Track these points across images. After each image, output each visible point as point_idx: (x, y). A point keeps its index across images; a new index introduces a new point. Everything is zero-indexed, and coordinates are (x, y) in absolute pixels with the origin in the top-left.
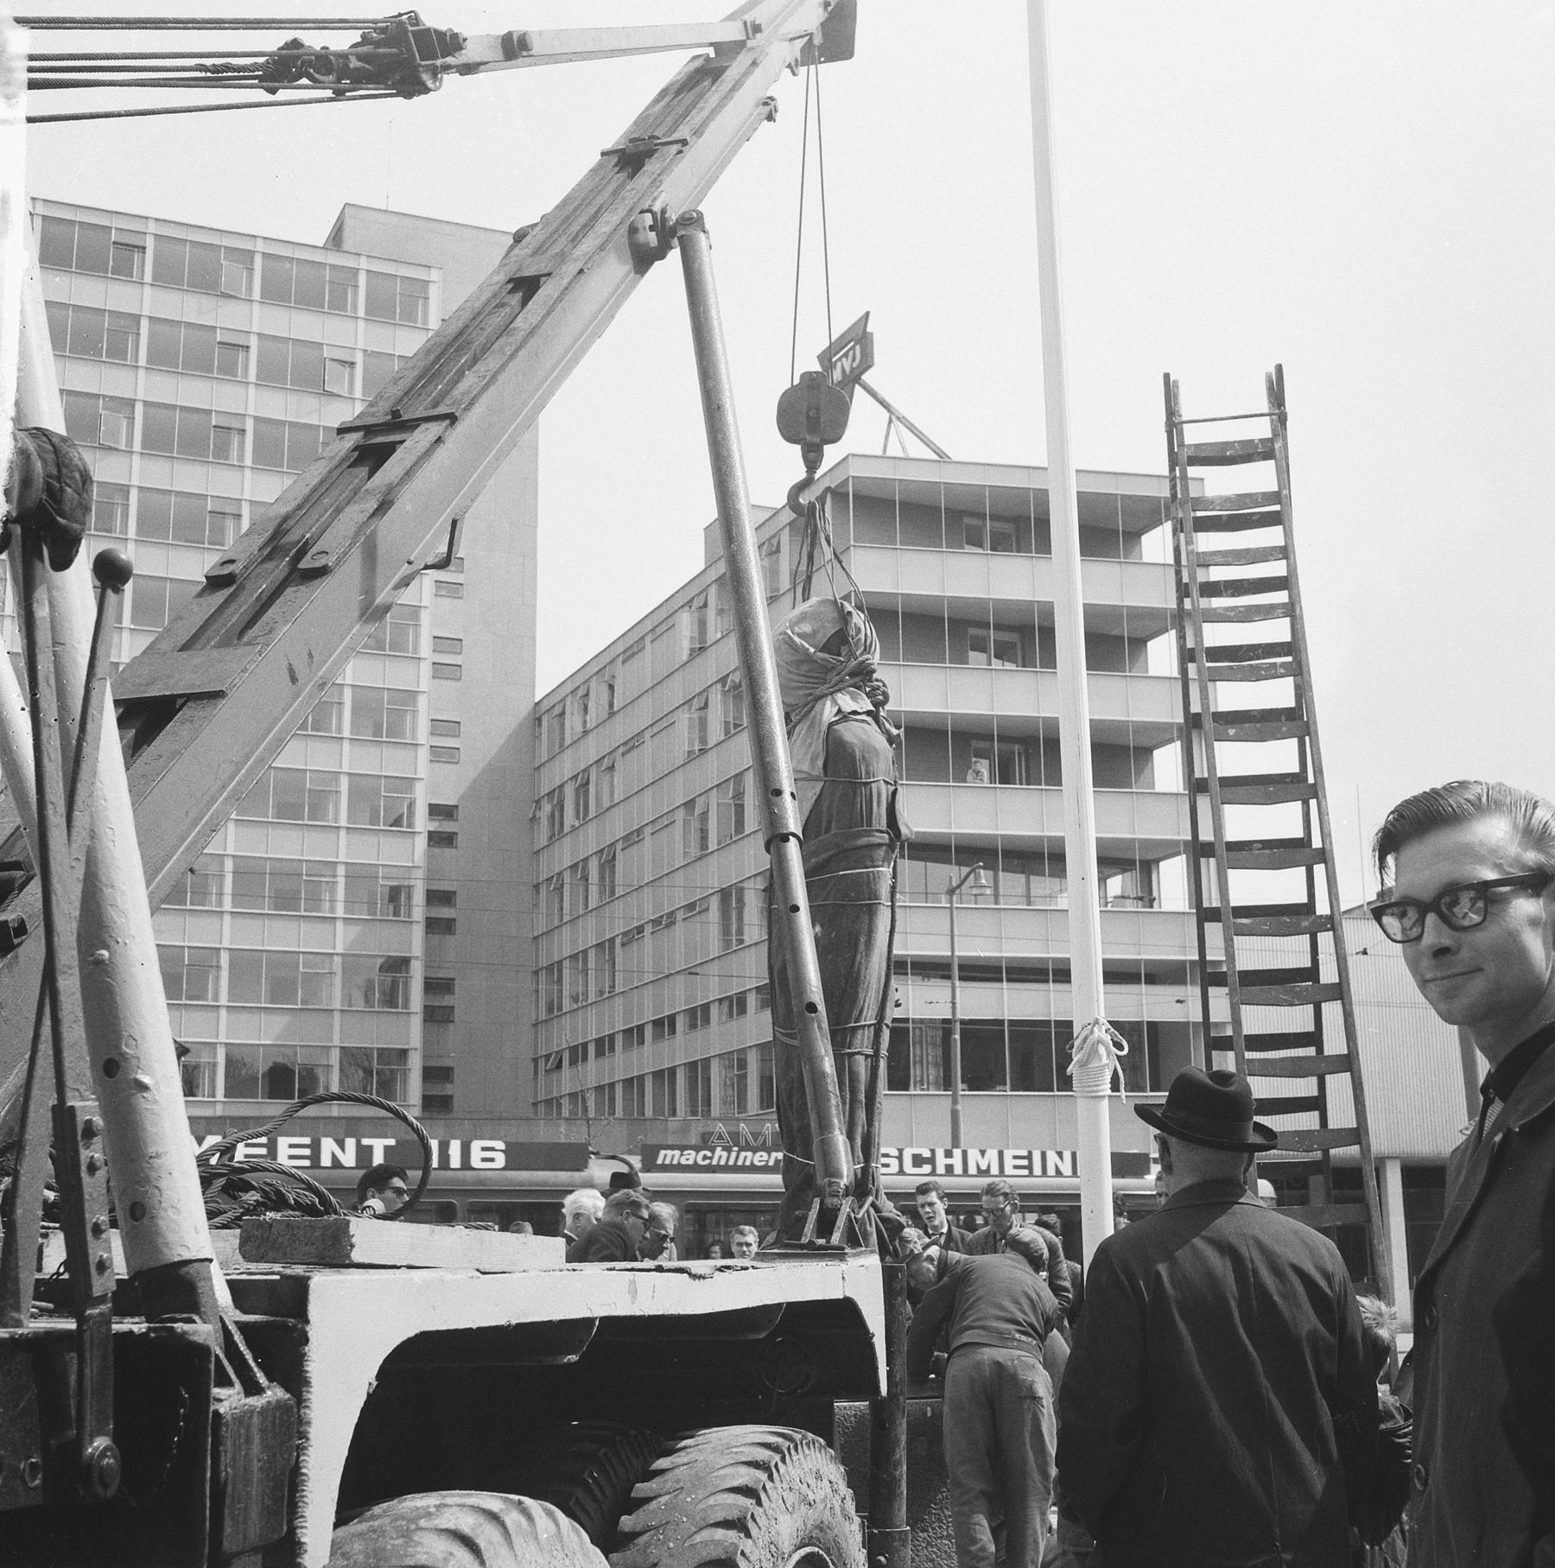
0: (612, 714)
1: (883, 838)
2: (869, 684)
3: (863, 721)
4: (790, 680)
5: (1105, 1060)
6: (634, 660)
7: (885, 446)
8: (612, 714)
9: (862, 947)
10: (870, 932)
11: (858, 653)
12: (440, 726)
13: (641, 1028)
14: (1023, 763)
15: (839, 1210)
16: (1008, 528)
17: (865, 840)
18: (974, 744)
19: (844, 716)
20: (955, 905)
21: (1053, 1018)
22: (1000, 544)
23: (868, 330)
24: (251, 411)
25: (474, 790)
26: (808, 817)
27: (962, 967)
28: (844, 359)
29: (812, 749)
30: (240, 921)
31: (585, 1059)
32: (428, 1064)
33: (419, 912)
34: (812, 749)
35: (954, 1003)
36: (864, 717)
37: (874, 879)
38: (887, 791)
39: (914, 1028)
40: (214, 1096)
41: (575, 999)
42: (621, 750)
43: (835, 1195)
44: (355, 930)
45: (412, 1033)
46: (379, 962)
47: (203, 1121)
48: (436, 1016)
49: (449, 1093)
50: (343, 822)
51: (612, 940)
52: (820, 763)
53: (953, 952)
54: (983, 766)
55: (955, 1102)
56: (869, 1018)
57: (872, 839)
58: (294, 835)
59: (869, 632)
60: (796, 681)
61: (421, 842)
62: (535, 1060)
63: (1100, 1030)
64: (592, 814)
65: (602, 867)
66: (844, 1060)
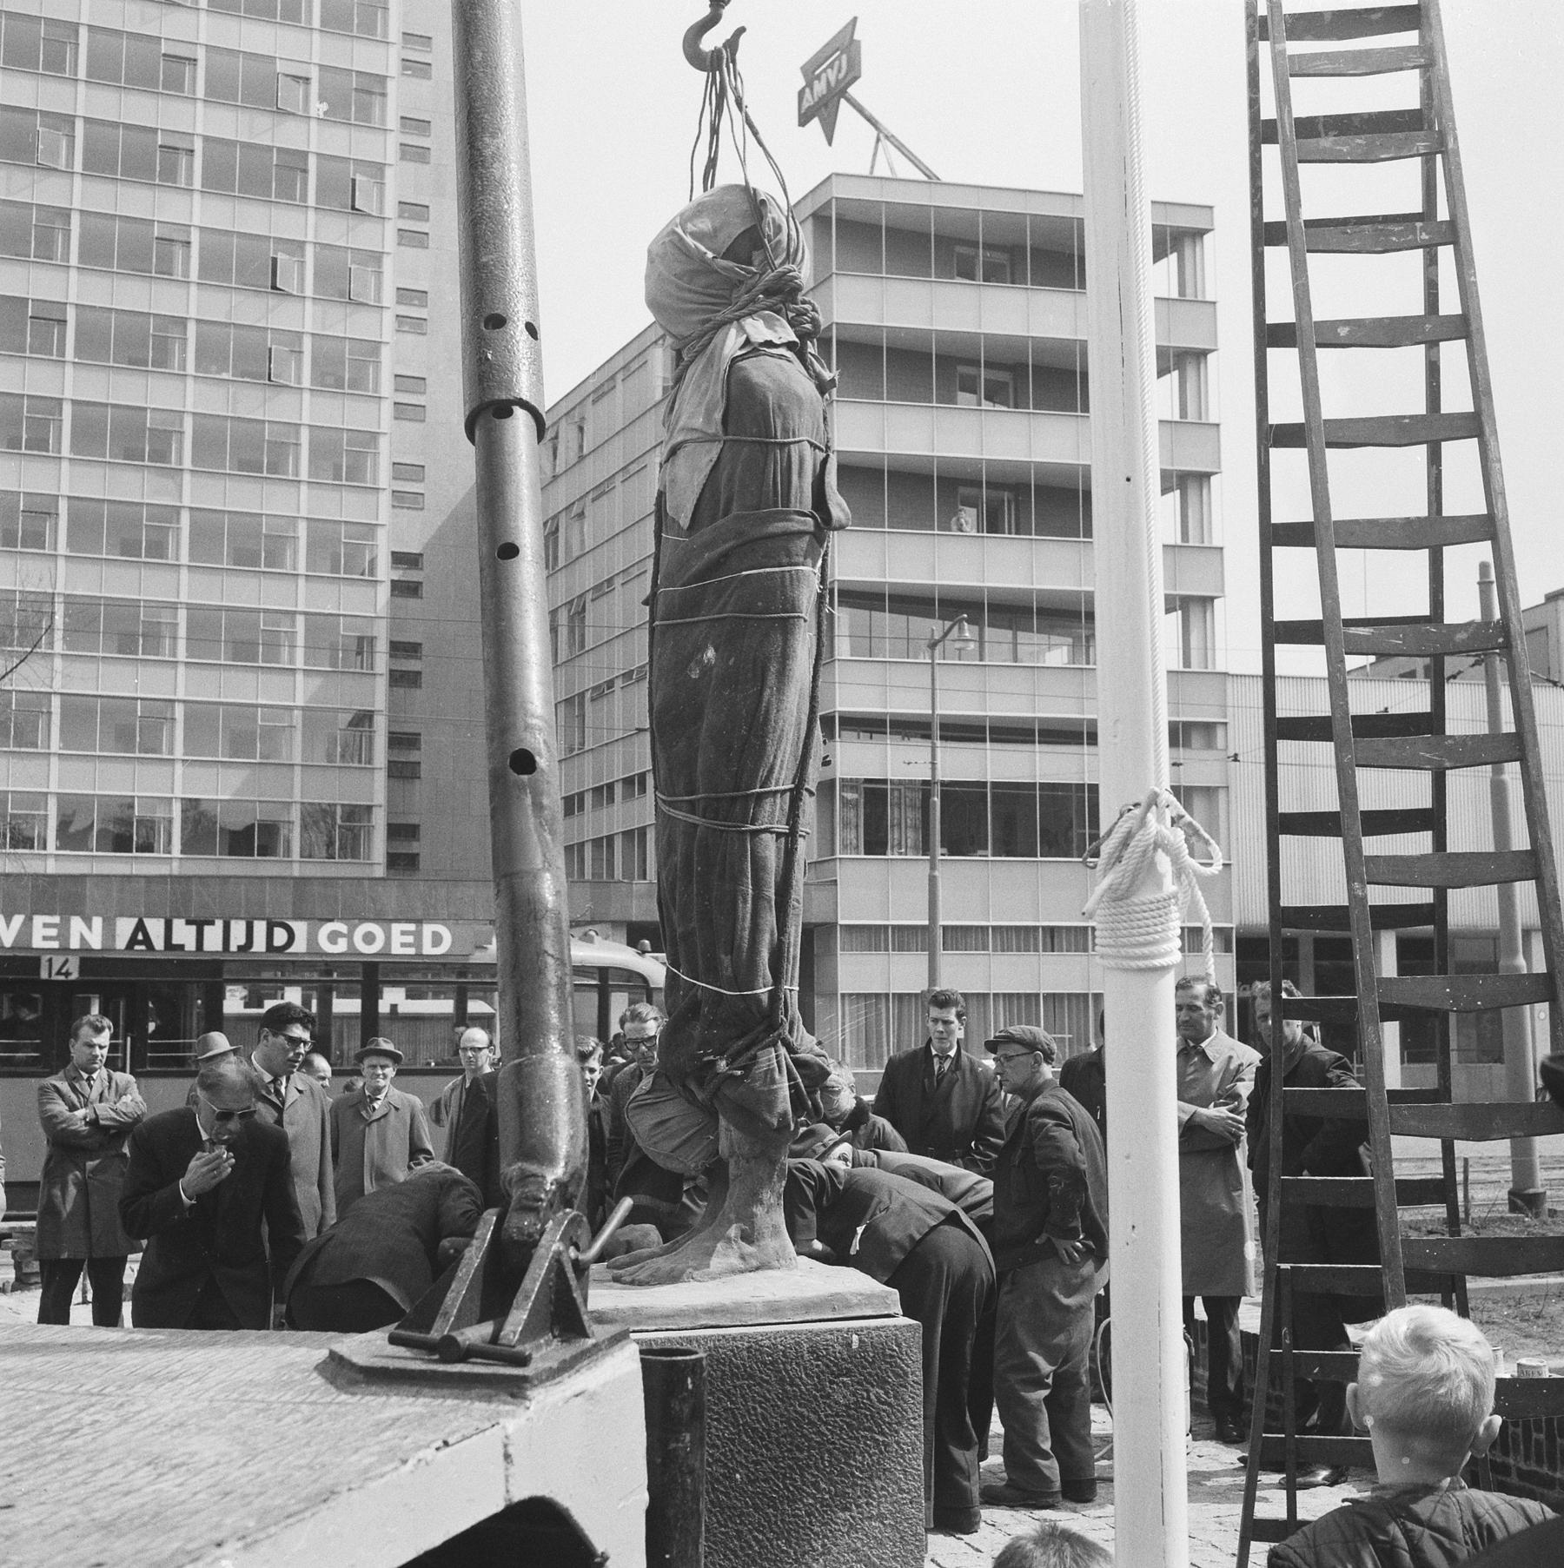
0: (582, 458)
1: (804, 523)
2: (792, 306)
3: (781, 357)
4: (686, 301)
5: (1169, 886)
6: (605, 399)
7: (872, 167)
8: (582, 458)
9: (772, 679)
10: (785, 658)
11: (777, 262)
12: (401, 470)
13: (610, 786)
14: (1013, 512)
15: (535, 1244)
16: (1000, 257)
17: (779, 526)
18: (962, 490)
19: (753, 349)
20: (937, 661)
21: (1038, 780)
22: (994, 274)
23: (856, 37)
24: (199, 130)
25: (440, 536)
26: (701, 494)
27: (943, 727)
28: (829, 70)
29: (708, 398)
30: (195, 672)
33: (382, 663)
34: (708, 398)
35: (933, 764)
36: (782, 351)
37: (791, 581)
38: (815, 460)
39: (892, 790)
40: (170, 853)
42: (591, 496)
43: (530, 1206)
44: (317, 682)
45: (376, 790)
46: (349, 717)
48: (401, 772)
49: (415, 851)
50: (302, 570)
51: (582, 695)
52: (718, 416)
53: (933, 709)
54: (968, 516)
55: (933, 868)
56: (783, 779)
57: (790, 524)
58: (252, 582)
59: (793, 233)
60: (691, 302)
61: (384, 592)
63: (1160, 819)
64: (561, 563)
65: (571, 619)
66: (744, 841)
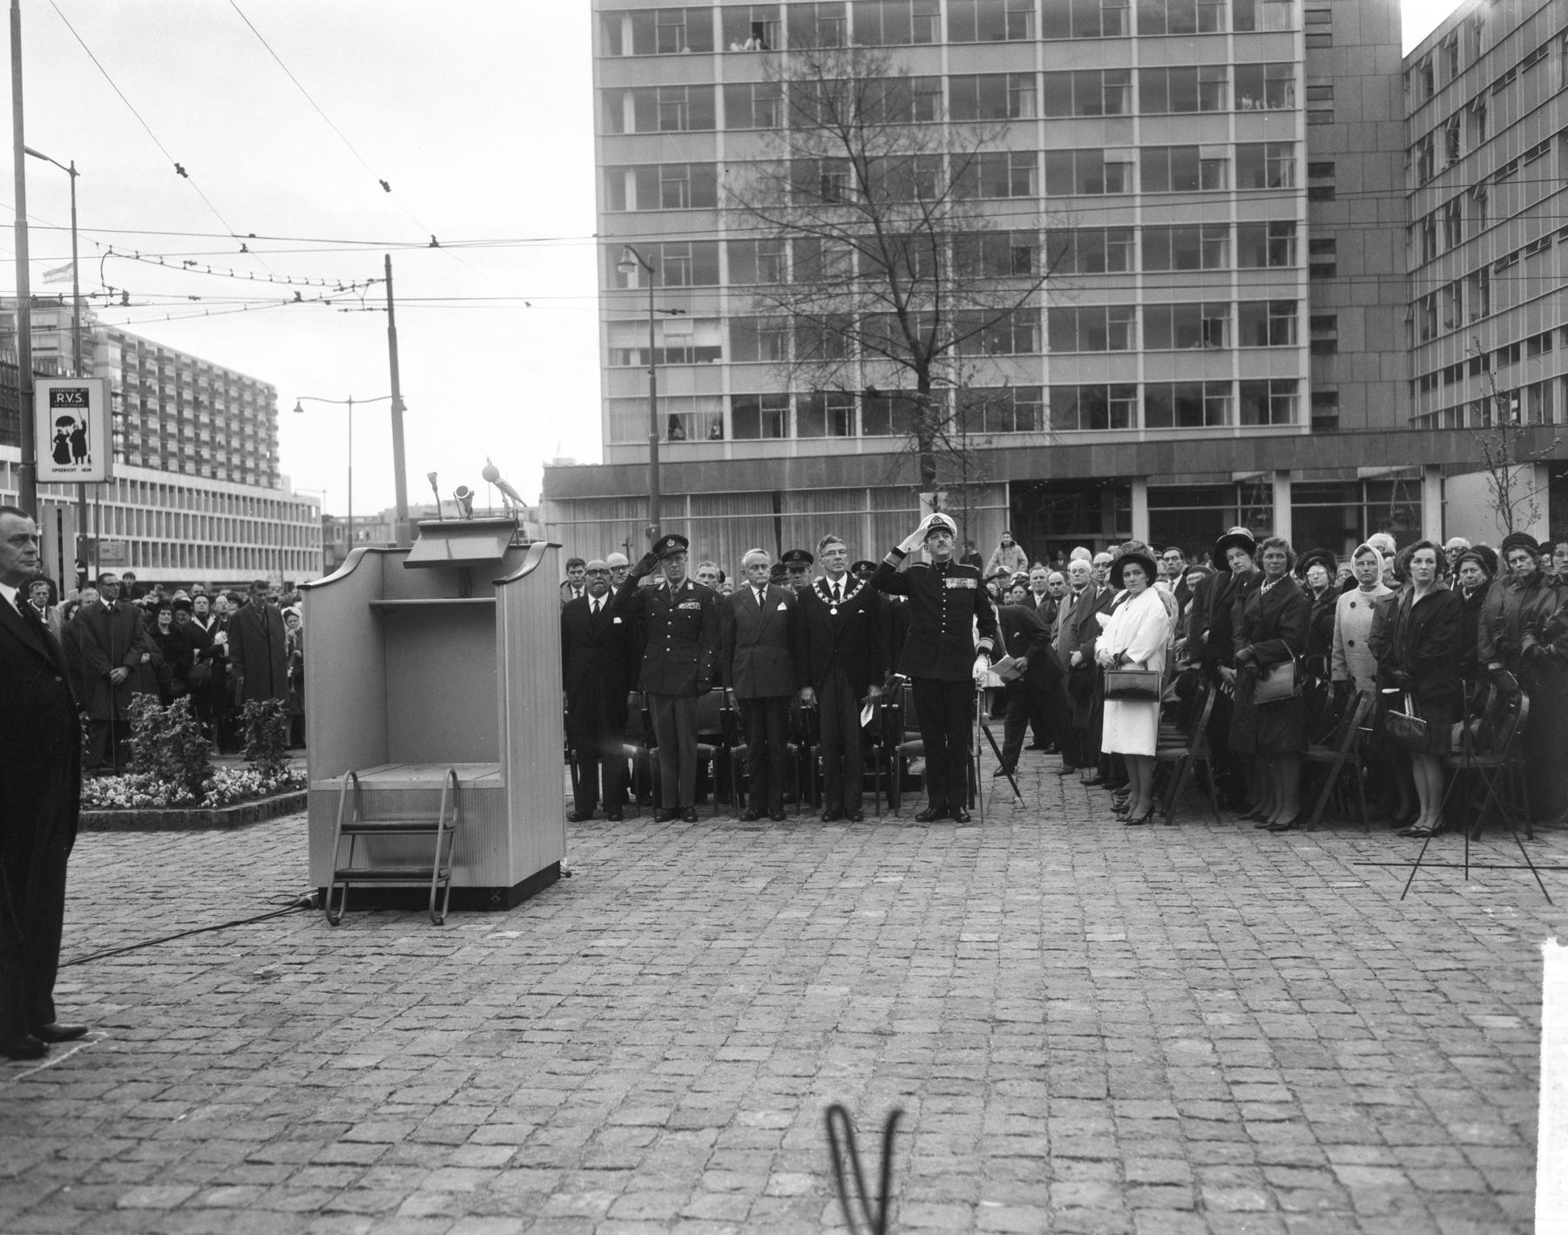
13: (1516, 347)
31: (1460, 377)
32: (1316, 314)
41: (1449, 325)
47: (1135, 447)
51: (1485, 270)
62: (1412, 382)
